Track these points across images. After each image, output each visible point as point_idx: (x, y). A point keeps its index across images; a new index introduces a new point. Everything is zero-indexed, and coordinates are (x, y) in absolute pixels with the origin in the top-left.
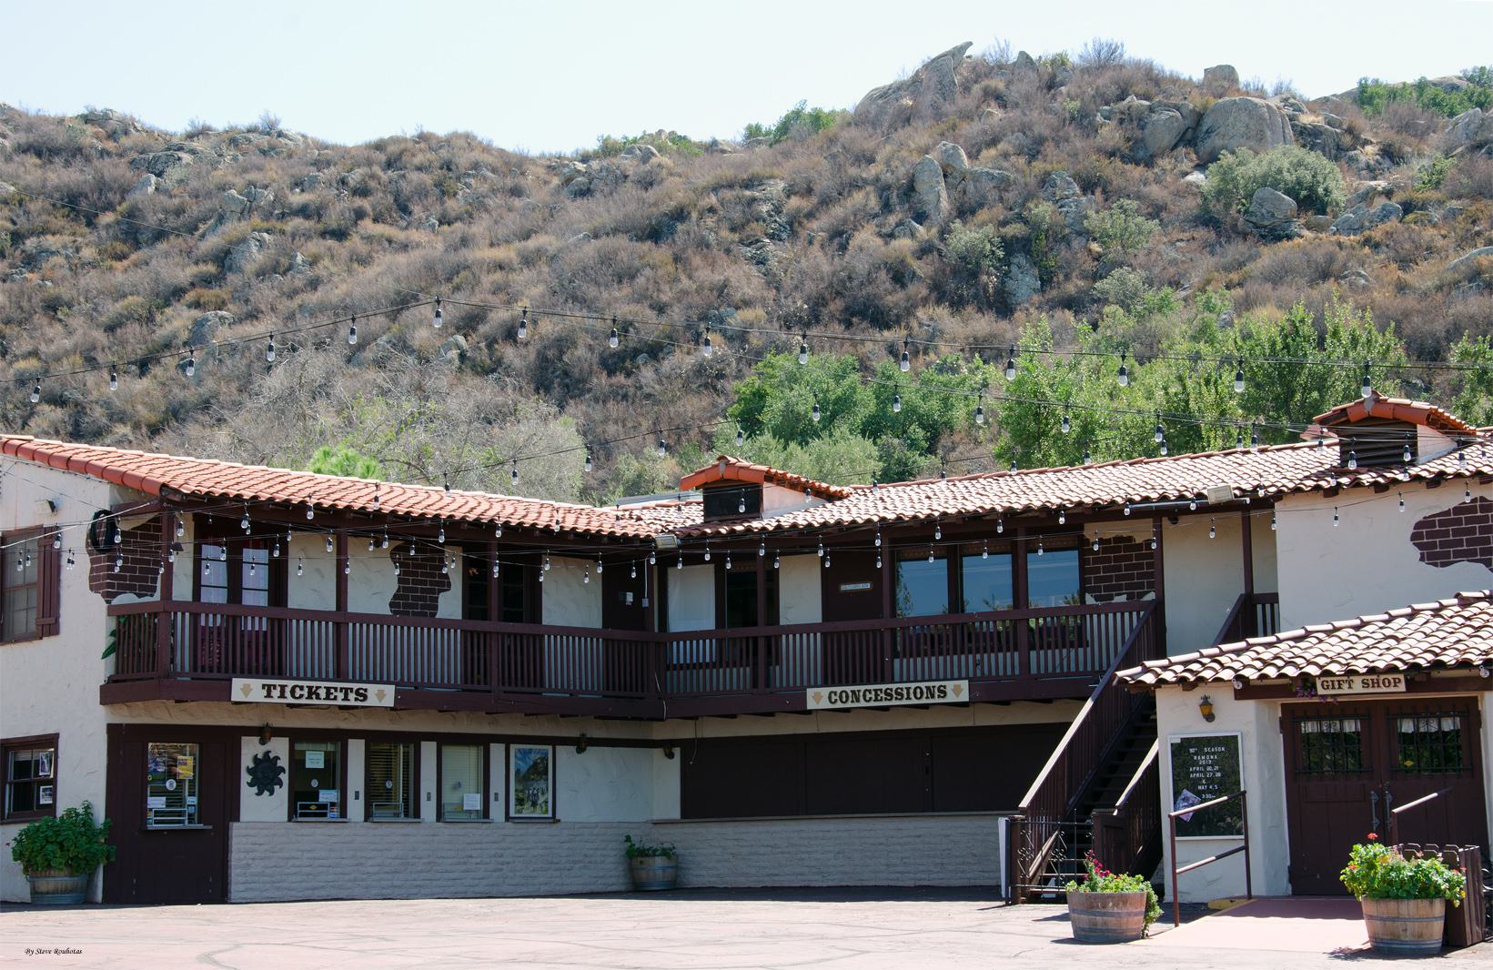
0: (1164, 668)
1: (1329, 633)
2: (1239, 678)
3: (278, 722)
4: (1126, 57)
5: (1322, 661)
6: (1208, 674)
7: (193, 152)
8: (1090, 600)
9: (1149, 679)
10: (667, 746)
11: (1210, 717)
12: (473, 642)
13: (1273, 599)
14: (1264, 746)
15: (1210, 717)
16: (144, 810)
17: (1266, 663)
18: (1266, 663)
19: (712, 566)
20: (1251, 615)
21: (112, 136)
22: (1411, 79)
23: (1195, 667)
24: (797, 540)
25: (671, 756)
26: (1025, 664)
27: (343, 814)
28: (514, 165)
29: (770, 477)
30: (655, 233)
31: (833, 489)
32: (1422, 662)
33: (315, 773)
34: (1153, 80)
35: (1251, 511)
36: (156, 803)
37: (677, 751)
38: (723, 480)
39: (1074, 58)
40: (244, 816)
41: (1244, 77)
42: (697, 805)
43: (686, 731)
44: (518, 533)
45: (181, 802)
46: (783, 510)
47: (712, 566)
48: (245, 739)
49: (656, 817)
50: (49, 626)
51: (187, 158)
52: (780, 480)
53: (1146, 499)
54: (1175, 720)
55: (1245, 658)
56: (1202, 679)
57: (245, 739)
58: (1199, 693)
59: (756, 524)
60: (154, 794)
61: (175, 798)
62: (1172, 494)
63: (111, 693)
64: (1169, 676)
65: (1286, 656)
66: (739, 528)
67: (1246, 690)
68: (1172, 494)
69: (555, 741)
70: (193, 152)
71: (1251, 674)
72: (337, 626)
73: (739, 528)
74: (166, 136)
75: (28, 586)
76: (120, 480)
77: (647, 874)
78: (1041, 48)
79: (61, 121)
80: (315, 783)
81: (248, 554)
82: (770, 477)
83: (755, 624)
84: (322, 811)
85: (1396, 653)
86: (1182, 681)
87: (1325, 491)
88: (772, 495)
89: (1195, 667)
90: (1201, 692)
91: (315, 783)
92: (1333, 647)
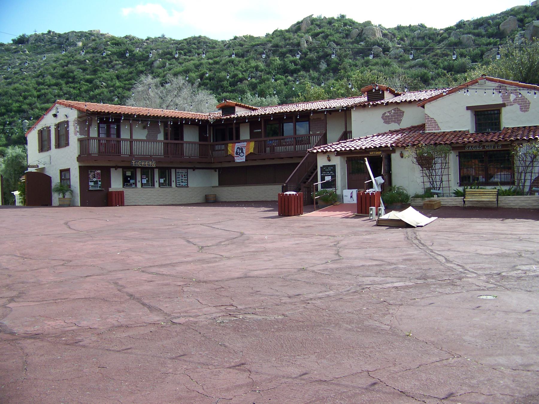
0: (319, 149)
1: (359, 140)
2: (336, 151)
3: (119, 165)
4: (347, 18)
5: (355, 146)
6: (329, 150)
7: (147, 43)
8: (311, 133)
9: (315, 151)
10: (215, 169)
11: (329, 160)
12: (166, 145)
13: (351, 132)
14: (342, 168)
15: (329, 160)
16: (88, 186)
17: (343, 147)
18: (343, 147)
19: (249, 124)
20: (346, 136)
21: (130, 40)
22: (452, 23)
23: (326, 148)
24: (242, 120)
25: (216, 171)
26: (295, 148)
27: (136, 186)
28: (215, 42)
29: (237, 105)
30: (243, 56)
31: (254, 107)
32: (378, 147)
33: (129, 177)
34: (352, 23)
35: (346, 111)
36: (92, 184)
37: (217, 170)
38: (226, 106)
39: (336, 18)
40: (112, 187)
41: (412, 25)
42: (222, 183)
43: (219, 166)
44: (175, 120)
45: (97, 184)
46: (240, 112)
47: (249, 124)
48: (112, 169)
49: (213, 185)
50: (67, 144)
51: (145, 44)
52: (240, 106)
53: (322, 108)
54: (322, 162)
55: (338, 146)
56: (327, 151)
57: (112, 169)
58: (327, 154)
59: (232, 116)
60: (91, 182)
61: (96, 183)
62: (328, 107)
63: (79, 159)
64: (320, 150)
65: (347, 145)
66: (228, 117)
67: (339, 153)
68: (328, 107)
69: (187, 168)
70: (147, 43)
71: (339, 150)
72: (131, 142)
73: (228, 117)
74: (142, 40)
75: (64, 135)
76: (80, 110)
77: (210, 201)
78: (328, 16)
79: (120, 38)
80: (129, 179)
81: (112, 126)
82: (237, 105)
83: (261, 137)
84: (131, 185)
85: (372, 144)
86: (322, 151)
87: (362, 106)
88: (237, 109)
89: (326, 148)
90: (329, 155)
91: (129, 179)
92: (359, 143)
